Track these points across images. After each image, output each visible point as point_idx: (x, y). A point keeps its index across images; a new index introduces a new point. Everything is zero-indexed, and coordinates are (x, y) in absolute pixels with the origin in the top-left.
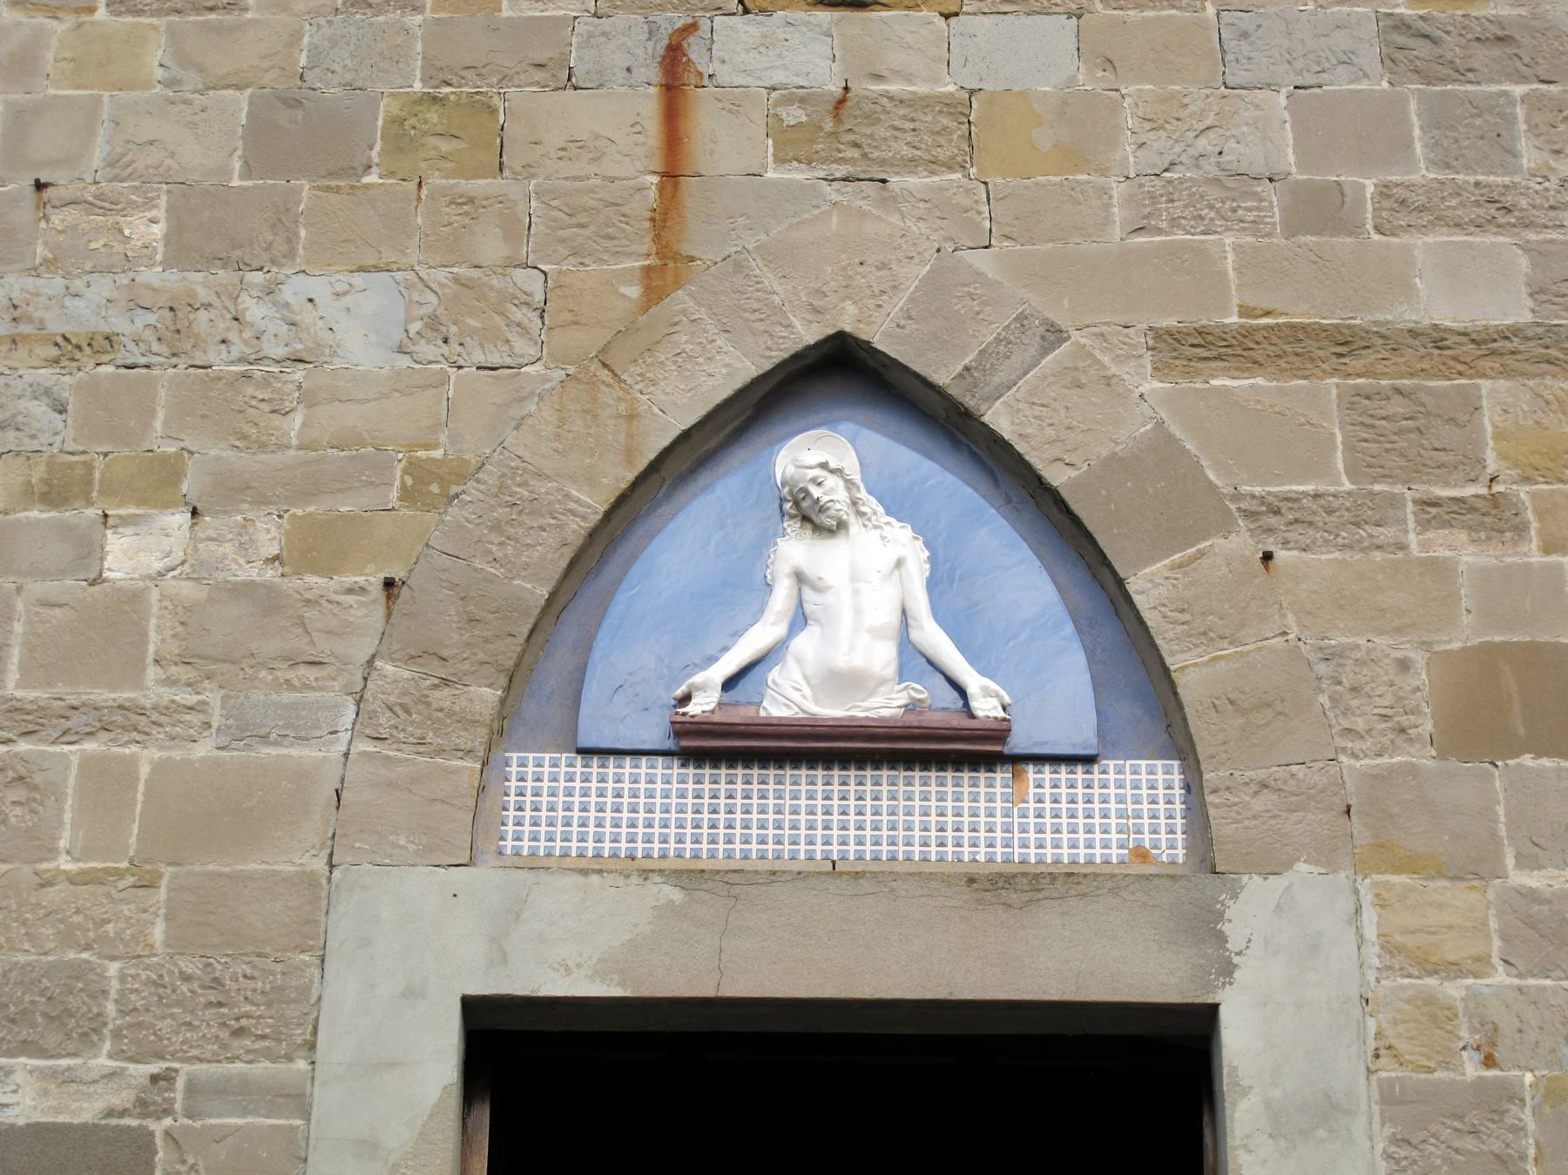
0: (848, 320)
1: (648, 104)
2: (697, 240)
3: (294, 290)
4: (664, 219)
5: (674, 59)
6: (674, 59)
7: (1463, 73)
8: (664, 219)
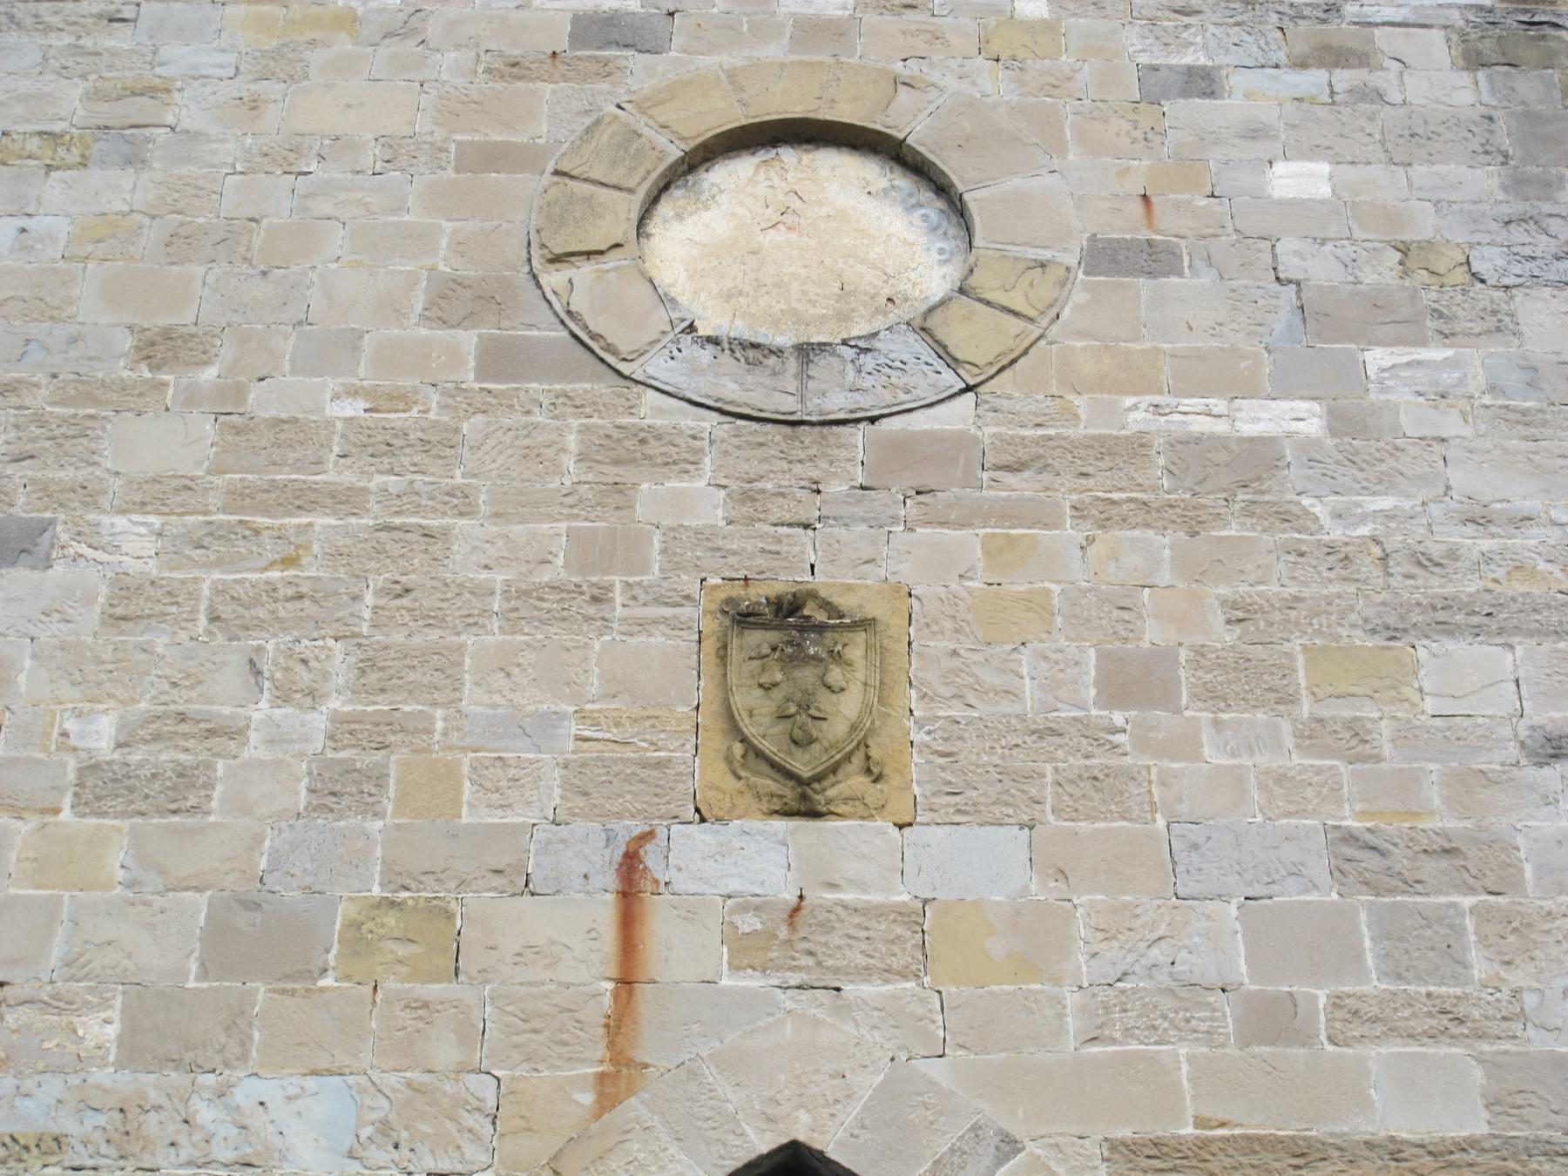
0: (802, 1130)
1: (605, 911)
2: (650, 1046)
3: (246, 1092)
4: (619, 1025)
5: (631, 865)
6: (631, 865)
7: (1412, 884)
8: (619, 1025)
